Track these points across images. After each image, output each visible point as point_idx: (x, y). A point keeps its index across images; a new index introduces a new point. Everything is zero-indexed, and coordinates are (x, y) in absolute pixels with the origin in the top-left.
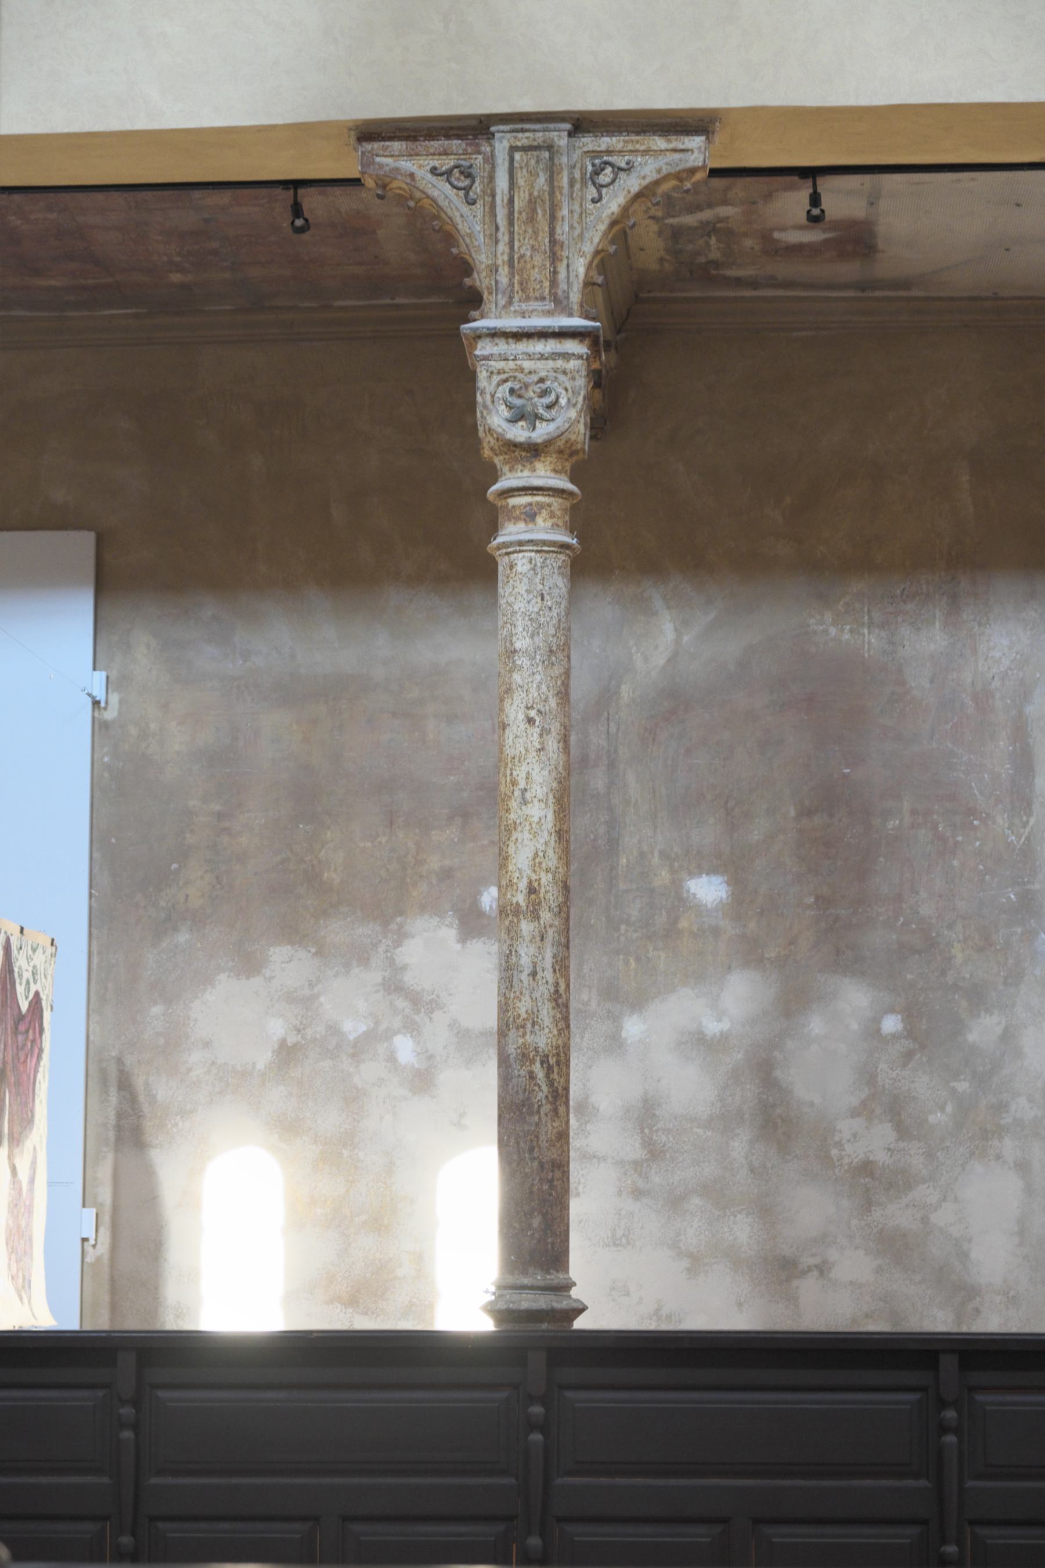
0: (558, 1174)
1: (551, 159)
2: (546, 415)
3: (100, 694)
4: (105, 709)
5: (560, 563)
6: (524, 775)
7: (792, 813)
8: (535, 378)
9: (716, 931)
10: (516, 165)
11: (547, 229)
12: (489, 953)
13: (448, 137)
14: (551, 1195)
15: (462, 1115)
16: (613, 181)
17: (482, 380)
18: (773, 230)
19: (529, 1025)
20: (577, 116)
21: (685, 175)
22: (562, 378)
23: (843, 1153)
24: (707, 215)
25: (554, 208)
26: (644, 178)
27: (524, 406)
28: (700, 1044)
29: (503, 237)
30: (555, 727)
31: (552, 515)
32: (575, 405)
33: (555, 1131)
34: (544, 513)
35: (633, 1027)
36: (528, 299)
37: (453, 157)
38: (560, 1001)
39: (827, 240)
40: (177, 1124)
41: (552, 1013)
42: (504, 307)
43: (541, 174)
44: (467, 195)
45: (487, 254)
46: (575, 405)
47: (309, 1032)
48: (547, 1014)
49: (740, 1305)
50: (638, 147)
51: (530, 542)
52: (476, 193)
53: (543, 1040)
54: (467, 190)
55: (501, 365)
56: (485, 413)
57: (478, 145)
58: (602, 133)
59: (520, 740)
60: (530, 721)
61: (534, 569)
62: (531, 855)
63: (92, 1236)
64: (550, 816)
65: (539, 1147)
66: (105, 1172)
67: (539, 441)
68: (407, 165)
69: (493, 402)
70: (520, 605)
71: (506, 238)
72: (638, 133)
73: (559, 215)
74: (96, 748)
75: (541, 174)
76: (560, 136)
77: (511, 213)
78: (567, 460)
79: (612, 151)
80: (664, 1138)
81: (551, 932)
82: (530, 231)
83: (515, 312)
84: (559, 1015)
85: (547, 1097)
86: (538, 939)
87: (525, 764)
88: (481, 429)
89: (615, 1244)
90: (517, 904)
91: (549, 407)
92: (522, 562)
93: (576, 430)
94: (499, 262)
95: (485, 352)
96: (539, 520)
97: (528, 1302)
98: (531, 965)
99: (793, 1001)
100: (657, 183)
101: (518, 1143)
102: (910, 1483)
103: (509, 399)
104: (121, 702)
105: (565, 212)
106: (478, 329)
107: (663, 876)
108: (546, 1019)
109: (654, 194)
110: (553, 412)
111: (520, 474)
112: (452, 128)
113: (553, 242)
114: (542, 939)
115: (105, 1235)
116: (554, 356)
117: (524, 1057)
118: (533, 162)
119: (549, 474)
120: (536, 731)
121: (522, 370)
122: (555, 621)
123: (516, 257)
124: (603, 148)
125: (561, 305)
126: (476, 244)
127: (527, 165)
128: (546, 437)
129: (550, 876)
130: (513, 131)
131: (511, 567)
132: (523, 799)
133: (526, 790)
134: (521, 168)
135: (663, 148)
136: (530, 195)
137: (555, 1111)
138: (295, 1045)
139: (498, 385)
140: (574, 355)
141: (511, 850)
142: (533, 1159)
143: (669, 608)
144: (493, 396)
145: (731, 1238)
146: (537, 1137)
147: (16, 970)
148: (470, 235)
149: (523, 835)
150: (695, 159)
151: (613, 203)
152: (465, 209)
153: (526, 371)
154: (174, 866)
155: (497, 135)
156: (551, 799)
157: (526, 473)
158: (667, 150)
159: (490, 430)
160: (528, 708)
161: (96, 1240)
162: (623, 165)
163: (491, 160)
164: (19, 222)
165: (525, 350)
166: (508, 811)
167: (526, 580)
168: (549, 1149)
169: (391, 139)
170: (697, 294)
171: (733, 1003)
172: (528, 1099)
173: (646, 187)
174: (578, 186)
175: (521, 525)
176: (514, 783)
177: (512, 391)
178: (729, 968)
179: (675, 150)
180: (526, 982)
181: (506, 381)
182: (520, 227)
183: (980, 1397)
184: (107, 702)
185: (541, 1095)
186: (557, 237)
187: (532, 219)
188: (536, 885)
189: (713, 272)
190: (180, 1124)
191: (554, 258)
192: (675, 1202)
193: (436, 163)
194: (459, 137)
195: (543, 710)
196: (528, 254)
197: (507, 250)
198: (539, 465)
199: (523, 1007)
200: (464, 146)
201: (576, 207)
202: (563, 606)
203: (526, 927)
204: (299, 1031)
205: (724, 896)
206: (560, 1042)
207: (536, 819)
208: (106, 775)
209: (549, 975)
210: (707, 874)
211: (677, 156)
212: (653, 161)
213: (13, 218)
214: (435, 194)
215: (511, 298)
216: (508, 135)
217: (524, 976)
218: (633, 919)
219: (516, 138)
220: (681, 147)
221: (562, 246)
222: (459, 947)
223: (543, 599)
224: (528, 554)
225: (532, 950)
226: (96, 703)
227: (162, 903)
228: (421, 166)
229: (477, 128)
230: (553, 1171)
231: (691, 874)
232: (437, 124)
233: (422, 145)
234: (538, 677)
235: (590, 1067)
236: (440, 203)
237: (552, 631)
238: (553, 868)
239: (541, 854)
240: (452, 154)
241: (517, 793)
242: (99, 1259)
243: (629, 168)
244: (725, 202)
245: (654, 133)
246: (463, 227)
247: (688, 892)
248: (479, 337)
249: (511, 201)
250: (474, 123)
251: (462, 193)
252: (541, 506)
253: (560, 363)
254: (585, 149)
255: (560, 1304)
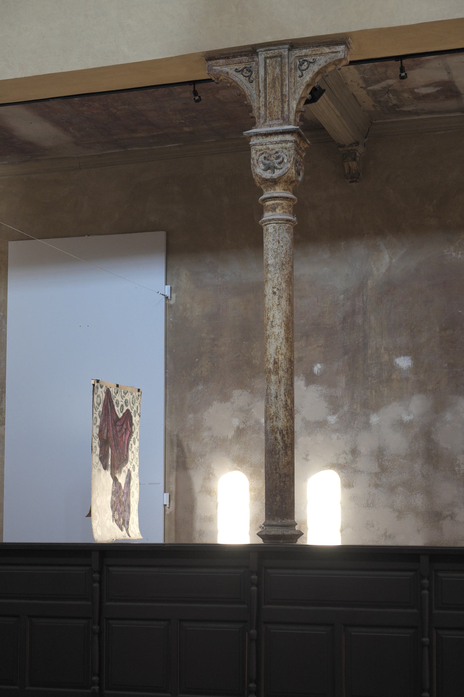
0: (287, 479)
1: (281, 61)
2: (279, 167)
3: (168, 293)
4: (171, 300)
5: (286, 228)
6: (272, 315)
7: (438, 330)
8: (274, 152)
9: (407, 379)
10: (267, 65)
11: (280, 90)
12: (317, 391)
13: (241, 56)
14: (284, 487)
15: (307, 455)
16: (307, 68)
17: (253, 154)
18: (414, 88)
19: (275, 418)
20: (291, 42)
21: (337, 62)
22: (285, 151)
23: (460, 469)
24: (384, 84)
25: (283, 80)
26: (320, 65)
27: (269, 164)
28: (401, 425)
29: (262, 95)
30: (285, 295)
31: (283, 208)
32: (290, 162)
33: (286, 461)
34: (279, 207)
35: (374, 419)
36: (272, 119)
37: (244, 64)
38: (288, 408)
39: (438, 91)
40: (199, 460)
41: (284, 413)
42: (263, 123)
43: (277, 67)
44: (249, 79)
45: (257, 103)
46: (290, 162)
47: (248, 423)
48: (282, 414)
49: (419, 531)
50: (317, 52)
51: (273, 219)
52: (253, 78)
53: (281, 424)
54: (249, 77)
55: (260, 147)
56: (254, 167)
57: (253, 58)
58: (302, 48)
59: (270, 301)
60: (274, 293)
61: (275, 231)
62: (275, 348)
63: (168, 504)
64: (283, 332)
65: (279, 468)
66: (172, 479)
67: (276, 177)
68: (226, 69)
69: (258, 163)
70: (270, 246)
71: (263, 95)
72: (317, 47)
73: (285, 84)
74: (167, 314)
75: (277, 67)
76: (284, 51)
77: (265, 85)
78: (290, 185)
79: (307, 55)
80: (387, 463)
81: (283, 380)
82: (273, 91)
83: (267, 125)
84: (287, 414)
85: (282, 447)
86: (278, 382)
87: (272, 311)
88: (254, 174)
89: (368, 506)
90: (270, 368)
91: (280, 163)
92: (270, 228)
93: (291, 172)
94: (261, 105)
95: (254, 143)
96: (277, 210)
97: (274, 531)
98: (275, 393)
99: (439, 407)
100: (326, 67)
101: (271, 466)
102: (409, 611)
103: (264, 161)
104: (176, 297)
105: (287, 82)
106: (250, 133)
107: (386, 357)
108: (281, 415)
109: (325, 72)
110: (282, 165)
111: (270, 192)
112: (242, 52)
113: (282, 95)
114: (280, 383)
115: (173, 503)
116: (281, 142)
117: (273, 431)
118: (274, 63)
119: (281, 191)
120: (277, 297)
121: (269, 149)
122: (284, 252)
123: (268, 103)
124: (303, 54)
125: (286, 121)
126: (253, 99)
127: (272, 64)
128: (278, 176)
129: (283, 357)
130: (266, 51)
131: (267, 230)
132: (272, 325)
133: (273, 321)
134: (269, 66)
135: (327, 52)
136: (273, 76)
137: (286, 453)
138: (243, 428)
139: (260, 156)
140: (289, 141)
141: (268, 346)
142: (276, 473)
143: (387, 249)
144: (257, 160)
145: (415, 504)
146: (278, 464)
147: (114, 401)
148: (250, 95)
149: (272, 340)
150: (341, 55)
151: (308, 77)
152: (249, 85)
153: (271, 149)
154: (197, 360)
155: (260, 53)
156: (283, 325)
157: (272, 191)
158: (329, 53)
159: (257, 174)
160: (273, 288)
161: (169, 505)
162: (312, 61)
163: (257, 64)
164: (115, 111)
165: (270, 140)
166: (266, 330)
167: (272, 235)
168: (283, 469)
169: (219, 59)
170: (394, 120)
171: (414, 408)
172: (275, 448)
173: (321, 69)
174: (293, 71)
175: (270, 213)
176: (268, 319)
177: (265, 158)
178: (413, 394)
179: (332, 52)
180: (273, 400)
181: (263, 154)
182: (269, 90)
183: (440, 574)
184: (171, 297)
185: (280, 447)
186: (284, 93)
187: (274, 86)
188: (277, 360)
189: (397, 109)
190: (200, 460)
191: (283, 102)
192: (392, 489)
193: (237, 67)
194: (245, 55)
195: (279, 288)
196: (272, 101)
197: (264, 100)
198: (277, 188)
199: (273, 410)
200: (248, 59)
201: (293, 80)
202: (288, 245)
203: (273, 378)
204: (244, 423)
205: (410, 365)
206: (288, 425)
207: (277, 333)
208: (171, 325)
209: (283, 397)
210: (403, 356)
211: (334, 55)
212: (323, 58)
213: (112, 109)
214: (237, 79)
215: (266, 120)
216: (264, 52)
217: (273, 398)
218: (374, 375)
219: (267, 53)
220: (335, 50)
221: (286, 97)
222: (305, 388)
223: (279, 243)
224: (273, 225)
225: (276, 387)
226: (167, 298)
227: (193, 375)
228: (231, 69)
229: (252, 51)
230: (285, 478)
231: (397, 356)
232: (236, 51)
233: (230, 61)
234: (277, 275)
235: (357, 435)
236: (239, 83)
237: (283, 256)
238: (284, 353)
239: (279, 348)
240: (243, 63)
241: (269, 323)
242: (171, 513)
243: (314, 62)
244: (388, 78)
245: (324, 46)
246: (248, 93)
247: (396, 363)
248: (251, 136)
249: (265, 80)
250: (251, 49)
251: (247, 78)
252: (278, 205)
253: (284, 145)
254: (296, 56)
255: (290, 532)
